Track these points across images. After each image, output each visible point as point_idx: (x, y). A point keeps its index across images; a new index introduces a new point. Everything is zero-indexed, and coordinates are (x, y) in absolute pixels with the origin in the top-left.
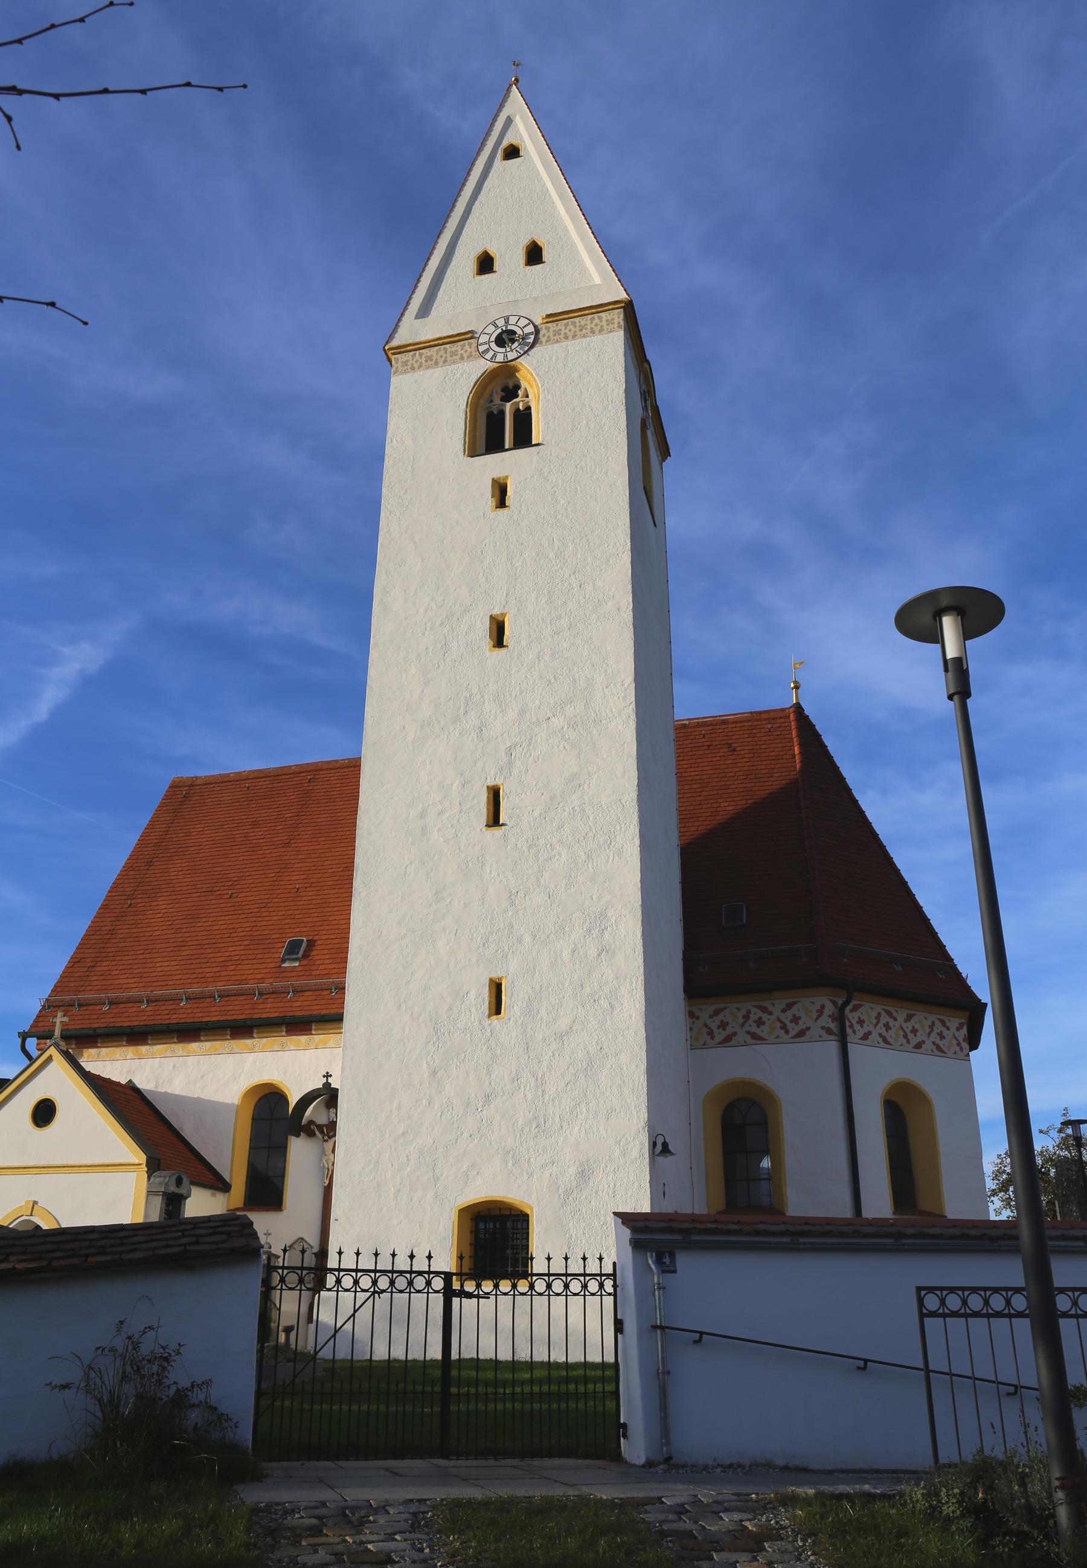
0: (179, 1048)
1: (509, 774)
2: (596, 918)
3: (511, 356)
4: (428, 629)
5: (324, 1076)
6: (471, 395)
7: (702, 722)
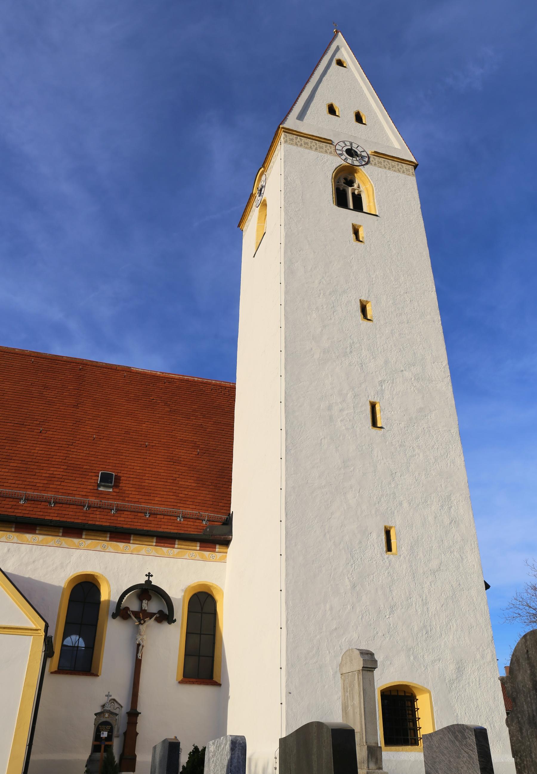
0: (15, 536)
3: (356, 163)
5: (146, 575)
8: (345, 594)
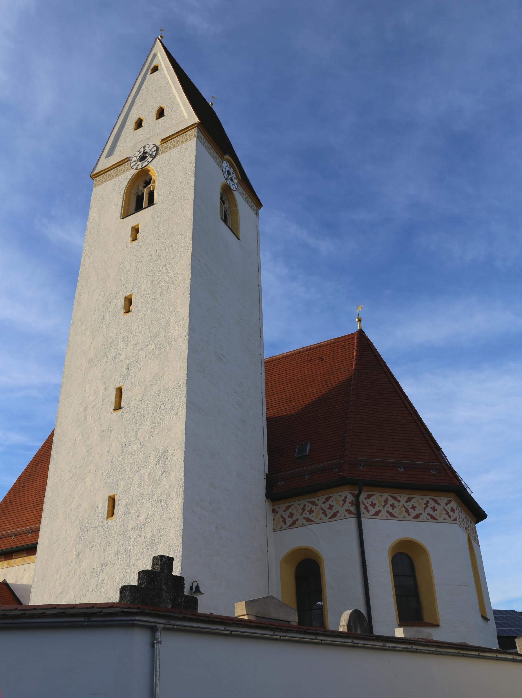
2: (162, 453)
4: (97, 310)
6: (126, 188)
7: (309, 348)
8: (71, 563)
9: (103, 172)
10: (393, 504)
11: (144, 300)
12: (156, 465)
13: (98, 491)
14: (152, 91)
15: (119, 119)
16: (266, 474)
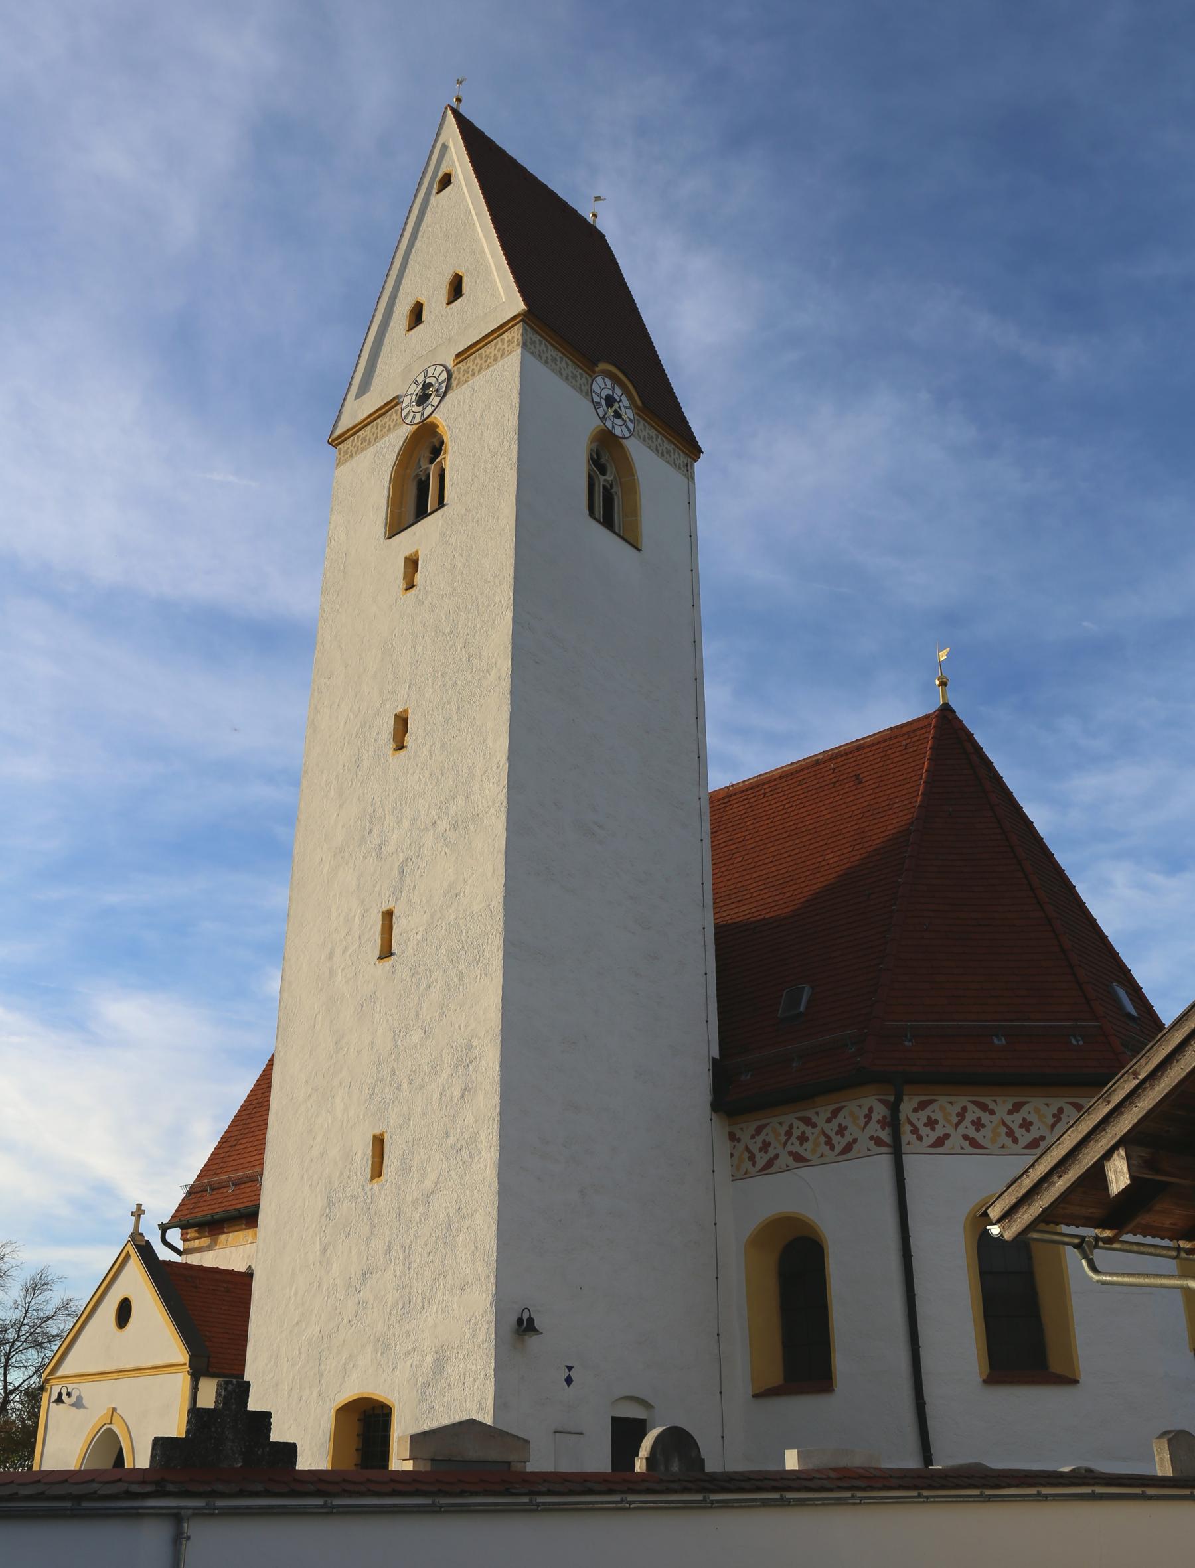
1: (400, 894)
2: (462, 1051)
9: (351, 432)
10: (979, 1119)
11: (429, 723)
12: (453, 1074)
13: (355, 1124)
14: (440, 235)
15: (379, 306)
16: (713, 1059)
